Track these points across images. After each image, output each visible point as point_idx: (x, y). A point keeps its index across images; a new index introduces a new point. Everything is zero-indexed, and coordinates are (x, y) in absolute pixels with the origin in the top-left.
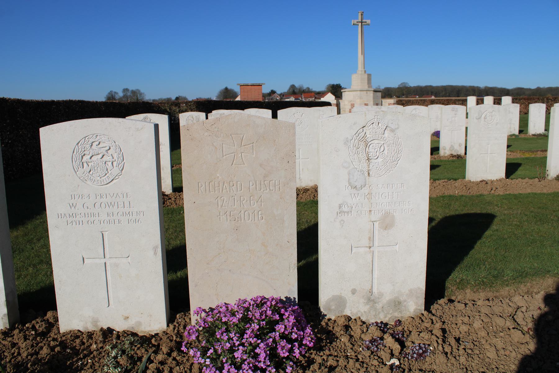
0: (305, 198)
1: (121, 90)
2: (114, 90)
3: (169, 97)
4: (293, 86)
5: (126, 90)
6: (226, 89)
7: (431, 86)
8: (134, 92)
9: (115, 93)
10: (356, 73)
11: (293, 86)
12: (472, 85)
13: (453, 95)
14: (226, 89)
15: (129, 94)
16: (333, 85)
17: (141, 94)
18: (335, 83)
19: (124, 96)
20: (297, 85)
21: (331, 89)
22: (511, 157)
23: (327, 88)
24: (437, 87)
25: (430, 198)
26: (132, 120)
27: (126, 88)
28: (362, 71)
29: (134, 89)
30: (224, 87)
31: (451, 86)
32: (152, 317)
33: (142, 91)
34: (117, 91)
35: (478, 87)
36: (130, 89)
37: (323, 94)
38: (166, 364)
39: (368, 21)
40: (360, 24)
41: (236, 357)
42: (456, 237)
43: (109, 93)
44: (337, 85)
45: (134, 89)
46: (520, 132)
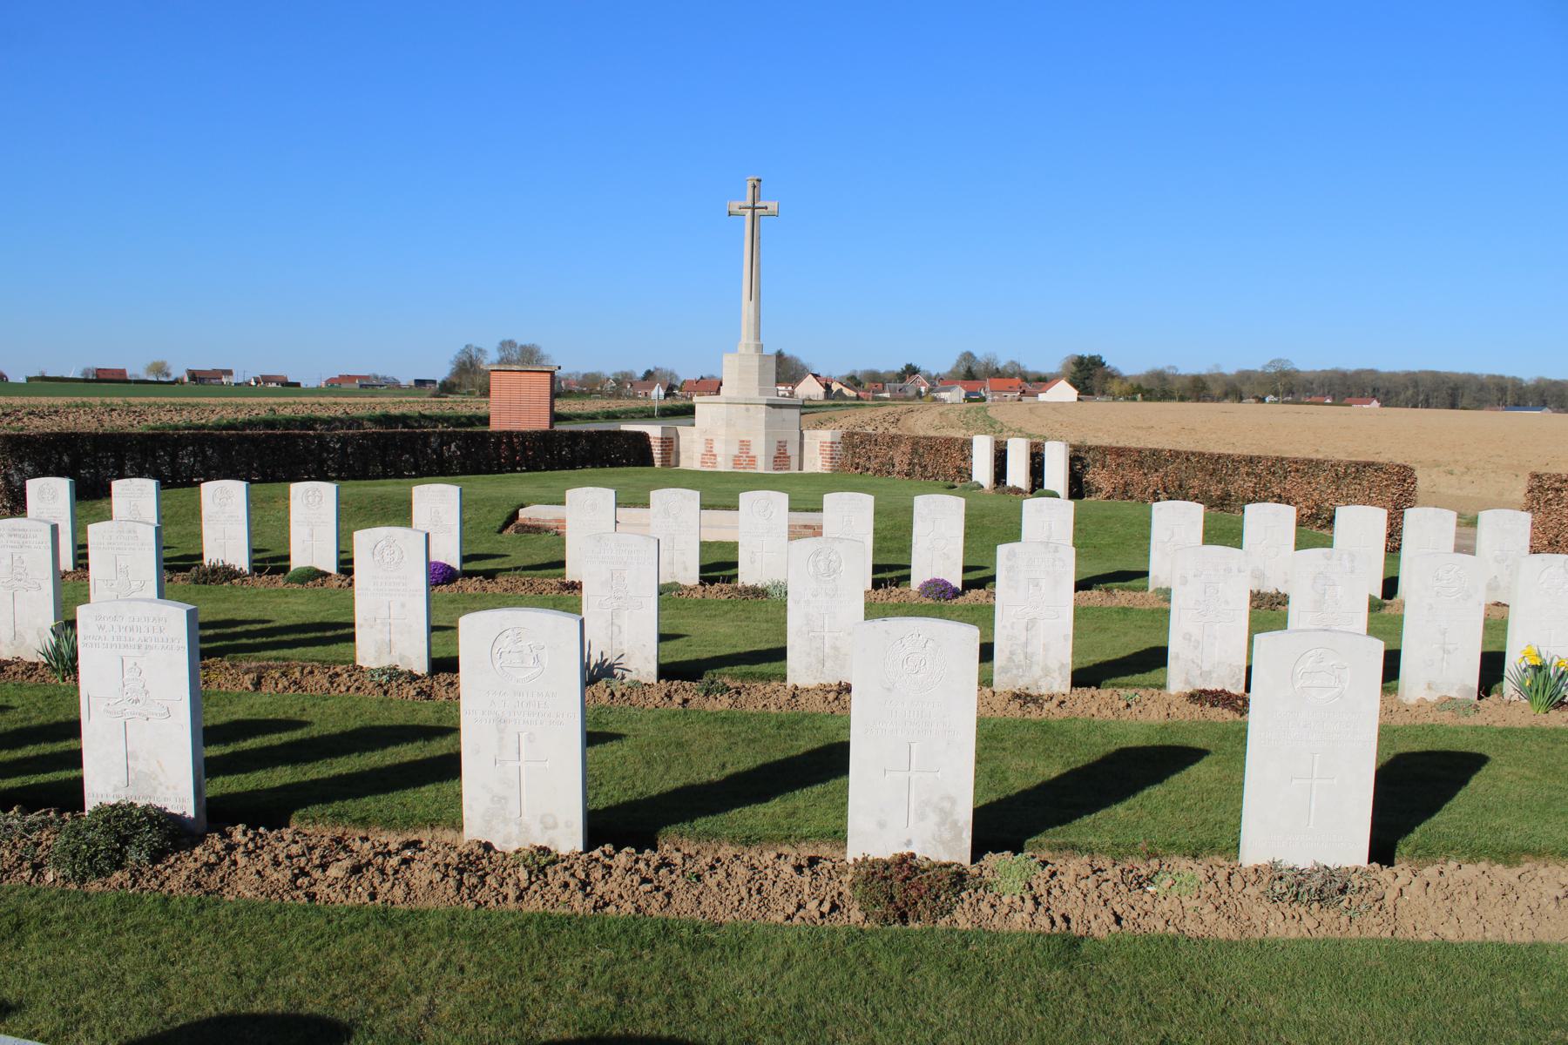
0: (1497, 613)
1: (496, 344)
2: (477, 343)
3: (626, 369)
4: (968, 356)
7: (1372, 372)
9: (480, 350)
10: (734, 350)
11: (968, 356)
16: (1081, 359)
18: (1087, 352)
20: (980, 354)
21: (1074, 369)
22: (777, 664)
23: (1066, 366)
24: (1394, 375)
25: (981, 722)
27: (507, 338)
28: (747, 345)
31: (1435, 374)
35: (1514, 379)
37: (1043, 381)
39: (772, 206)
40: (749, 213)
42: (1416, 787)
43: (463, 352)
44: (1092, 358)
46: (1473, 523)
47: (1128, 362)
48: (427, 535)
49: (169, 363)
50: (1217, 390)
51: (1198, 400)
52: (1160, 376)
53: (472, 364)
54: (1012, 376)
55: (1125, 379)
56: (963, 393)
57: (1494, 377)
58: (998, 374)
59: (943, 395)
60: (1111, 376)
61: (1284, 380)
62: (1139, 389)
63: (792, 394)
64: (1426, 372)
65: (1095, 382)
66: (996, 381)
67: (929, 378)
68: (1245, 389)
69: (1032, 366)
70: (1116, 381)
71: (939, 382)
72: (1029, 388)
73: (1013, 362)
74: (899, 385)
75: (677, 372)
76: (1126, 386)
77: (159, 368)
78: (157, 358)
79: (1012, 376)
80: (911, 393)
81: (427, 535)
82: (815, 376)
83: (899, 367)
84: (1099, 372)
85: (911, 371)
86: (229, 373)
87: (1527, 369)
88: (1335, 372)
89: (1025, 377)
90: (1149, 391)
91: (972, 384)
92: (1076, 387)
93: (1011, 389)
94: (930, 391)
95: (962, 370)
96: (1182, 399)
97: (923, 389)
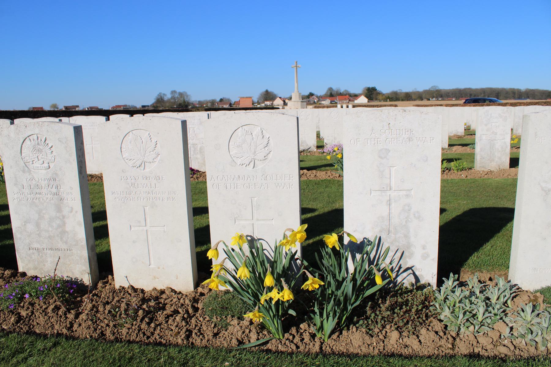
1: (170, 92)
2: (163, 92)
3: (213, 98)
4: (330, 89)
5: (173, 92)
6: (267, 91)
7: (470, 89)
8: (181, 94)
9: (164, 94)
11: (330, 89)
12: (512, 87)
13: (476, 98)
14: (267, 91)
15: (176, 95)
17: (187, 96)
18: (371, 86)
19: (172, 98)
20: (335, 88)
21: (366, 92)
23: (364, 91)
24: (477, 89)
25: (208, 213)
26: (164, 117)
27: (173, 90)
29: (181, 91)
30: (265, 90)
31: (491, 89)
32: (182, 279)
33: (189, 93)
34: (165, 93)
36: (178, 91)
37: (356, 96)
38: (251, 320)
41: (183, 321)
43: (158, 95)
45: (181, 91)
47: (385, 89)
48: (298, 118)
49: (58, 104)
50: (413, 97)
51: (408, 100)
52: (395, 93)
53: (161, 99)
54: (346, 95)
55: (384, 94)
56: (329, 101)
57: (511, 89)
58: (341, 94)
59: (323, 102)
60: (379, 93)
61: (436, 93)
62: (388, 98)
63: (272, 104)
64: (488, 88)
65: (374, 96)
66: (341, 97)
67: (317, 97)
68: (424, 96)
69: (353, 91)
70: (381, 95)
71: (320, 98)
72: (351, 98)
73: (346, 90)
74: (308, 100)
75: (231, 99)
76: (384, 97)
77: (55, 106)
78: (54, 102)
79: (346, 95)
80: (312, 102)
81: (298, 118)
82: (280, 98)
83: (307, 93)
84: (375, 92)
85: (311, 95)
86: (78, 106)
87: (523, 86)
88: (457, 89)
89: (350, 95)
90: (392, 98)
91: (332, 98)
92: (367, 98)
93: (345, 99)
94: (318, 101)
95: (329, 94)
96: (402, 100)
97: (316, 101)
